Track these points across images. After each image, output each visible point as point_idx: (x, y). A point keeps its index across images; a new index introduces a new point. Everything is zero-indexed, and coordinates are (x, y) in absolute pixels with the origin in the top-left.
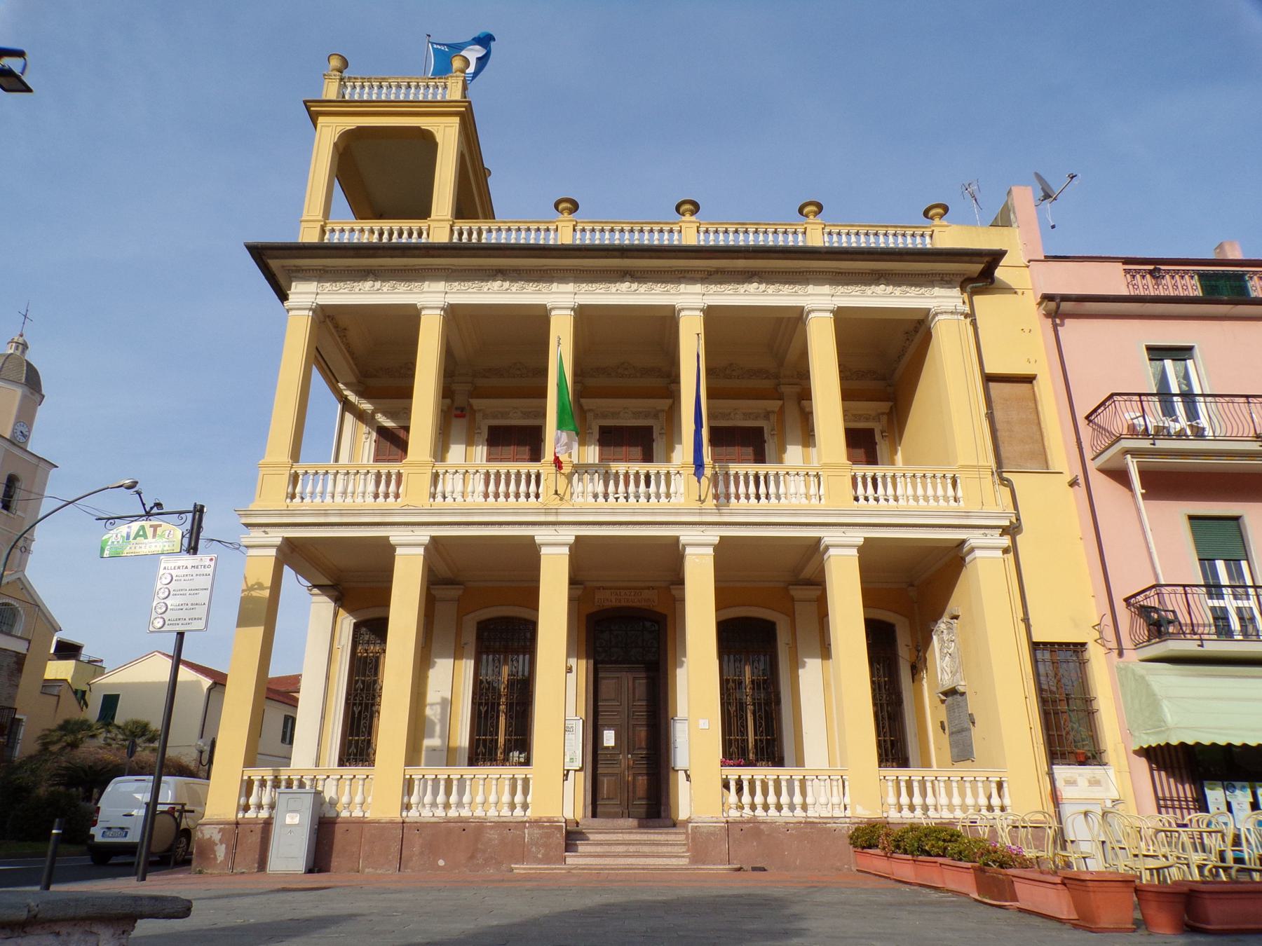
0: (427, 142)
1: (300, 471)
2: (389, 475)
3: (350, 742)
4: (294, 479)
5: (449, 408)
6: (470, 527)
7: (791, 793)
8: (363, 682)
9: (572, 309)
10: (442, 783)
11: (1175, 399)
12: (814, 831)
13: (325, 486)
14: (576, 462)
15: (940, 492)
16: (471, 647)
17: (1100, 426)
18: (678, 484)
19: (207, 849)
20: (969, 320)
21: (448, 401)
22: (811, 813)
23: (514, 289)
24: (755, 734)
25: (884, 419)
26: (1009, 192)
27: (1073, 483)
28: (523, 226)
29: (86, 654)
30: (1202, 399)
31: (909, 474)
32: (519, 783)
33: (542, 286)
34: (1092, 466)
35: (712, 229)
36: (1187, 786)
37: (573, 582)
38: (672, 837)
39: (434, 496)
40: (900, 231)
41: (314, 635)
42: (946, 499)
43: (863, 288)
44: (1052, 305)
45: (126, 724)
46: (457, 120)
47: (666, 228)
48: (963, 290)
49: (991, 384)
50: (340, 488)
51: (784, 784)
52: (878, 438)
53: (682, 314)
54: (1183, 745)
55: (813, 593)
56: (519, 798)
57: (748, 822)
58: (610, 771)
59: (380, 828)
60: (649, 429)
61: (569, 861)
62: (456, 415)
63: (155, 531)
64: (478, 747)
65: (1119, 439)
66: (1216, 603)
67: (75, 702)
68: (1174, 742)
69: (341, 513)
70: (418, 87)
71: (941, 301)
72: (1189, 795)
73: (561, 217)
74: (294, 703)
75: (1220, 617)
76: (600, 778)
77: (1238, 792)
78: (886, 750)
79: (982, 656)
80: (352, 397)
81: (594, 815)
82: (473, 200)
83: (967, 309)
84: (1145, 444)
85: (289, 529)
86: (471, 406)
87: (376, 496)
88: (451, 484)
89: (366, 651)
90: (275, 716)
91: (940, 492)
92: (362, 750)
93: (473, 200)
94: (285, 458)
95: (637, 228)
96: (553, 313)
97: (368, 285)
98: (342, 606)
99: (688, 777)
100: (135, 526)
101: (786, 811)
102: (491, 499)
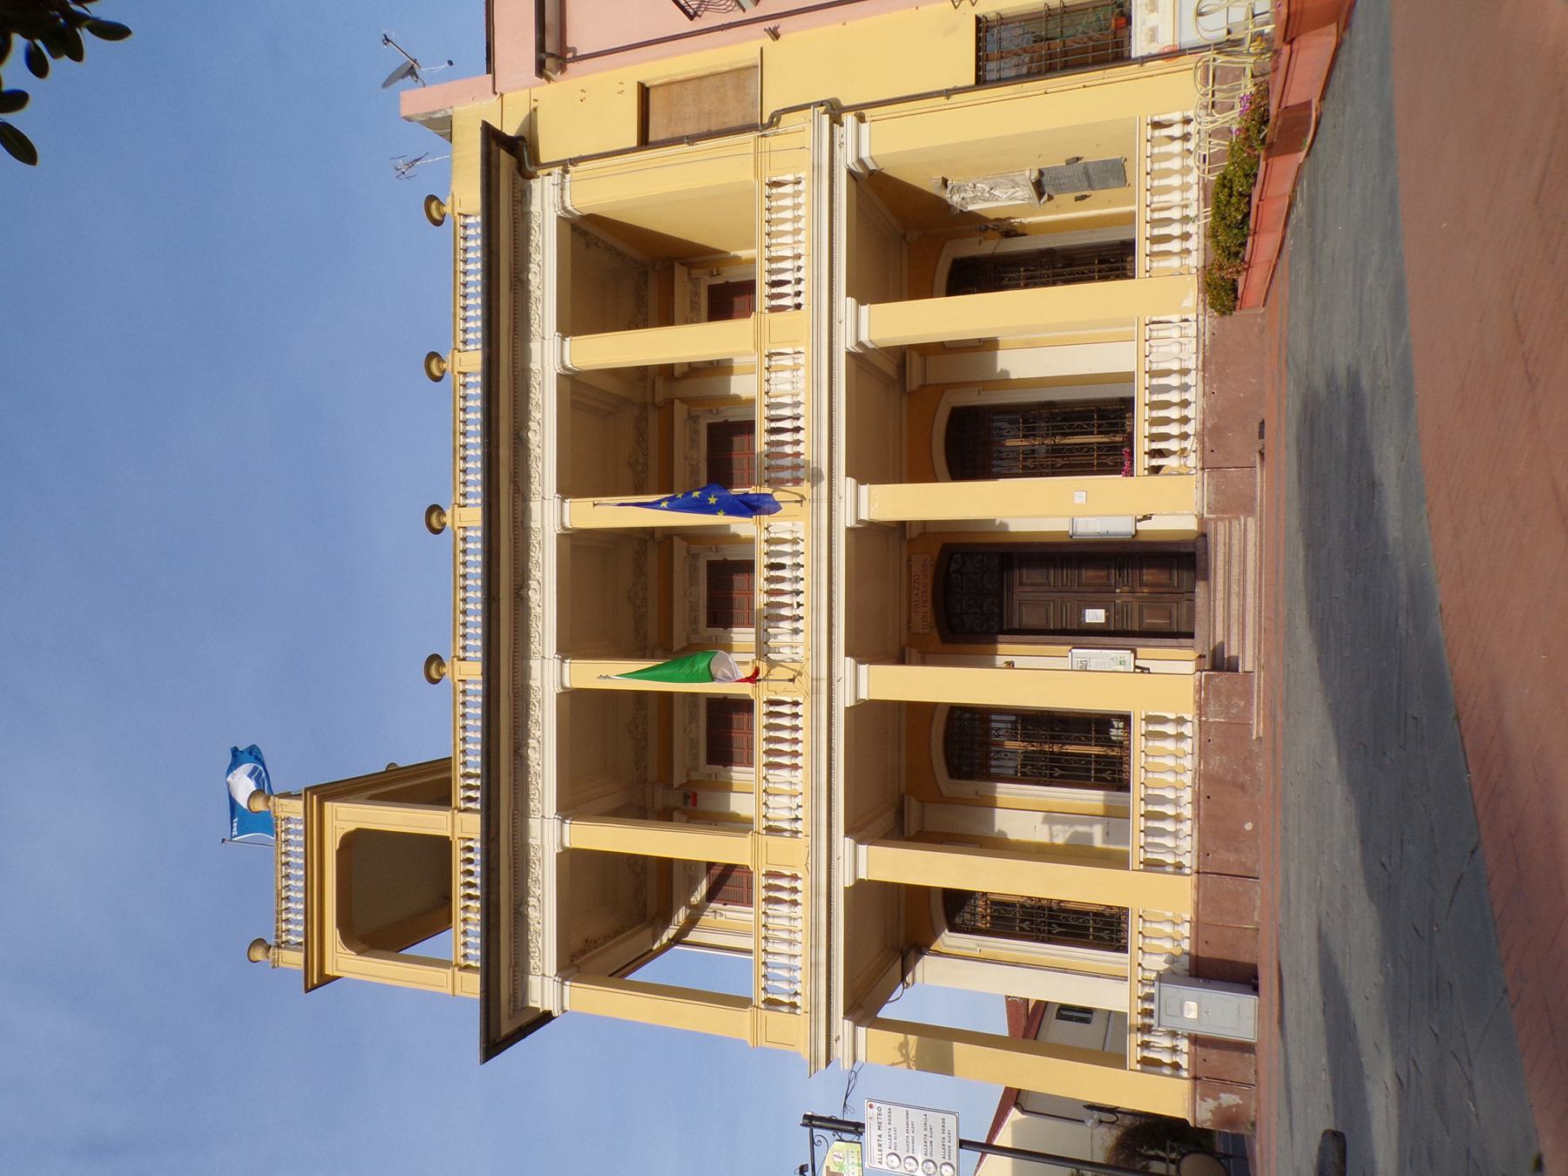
0: (355, 842)
1: (763, 996)
2: (768, 887)
3: (1096, 779)
4: (772, 1004)
5: (685, 813)
6: (835, 787)
8: (1022, 921)
10: (1150, 824)
12: (1214, 361)
15: (788, 202)
19: (1229, 1117)
20: (571, 168)
21: (676, 814)
22: (1191, 364)
23: (538, 733)
24: (1092, 433)
25: (696, 272)
26: (409, 119)
27: (775, 35)
28: (460, 722)
31: (767, 241)
32: (1151, 728)
35: (462, 489)
37: (901, 660)
38: (1221, 539)
40: (460, 256)
41: (963, 980)
42: (797, 194)
43: (533, 300)
44: (549, 62)
46: (328, 805)
47: (461, 546)
49: (652, 138)
51: (1155, 398)
53: (568, 525)
55: (914, 361)
56: (1170, 729)
57: (1202, 443)
58: (1136, 615)
59: (1204, 901)
60: (712, 565)
61: (1249, 667)
62: (693, 804)
64: (1104, 779)
69: (815, 947)
70: (287, 854)
71: (547, 203)
73: (448, 676)
74: (1042, 1006)
76: (1145, 627)
78: (1112, 270)
79: (993, 147)
80: (671, 932)
81: (1191, 635)
82: (428, 784)
83: (557, 170)
87: (794, 903)
88: (780, 810)
89: (984, 917)
90: (1057, 1030)
91: (788, 202)
92: (1107, 923)
93: (428, 784)
94: (746, 1015)
95: (461, 582)
96: (567, 685)
98: (928, 946)
99: (1146, 518)
102: (799, 761)
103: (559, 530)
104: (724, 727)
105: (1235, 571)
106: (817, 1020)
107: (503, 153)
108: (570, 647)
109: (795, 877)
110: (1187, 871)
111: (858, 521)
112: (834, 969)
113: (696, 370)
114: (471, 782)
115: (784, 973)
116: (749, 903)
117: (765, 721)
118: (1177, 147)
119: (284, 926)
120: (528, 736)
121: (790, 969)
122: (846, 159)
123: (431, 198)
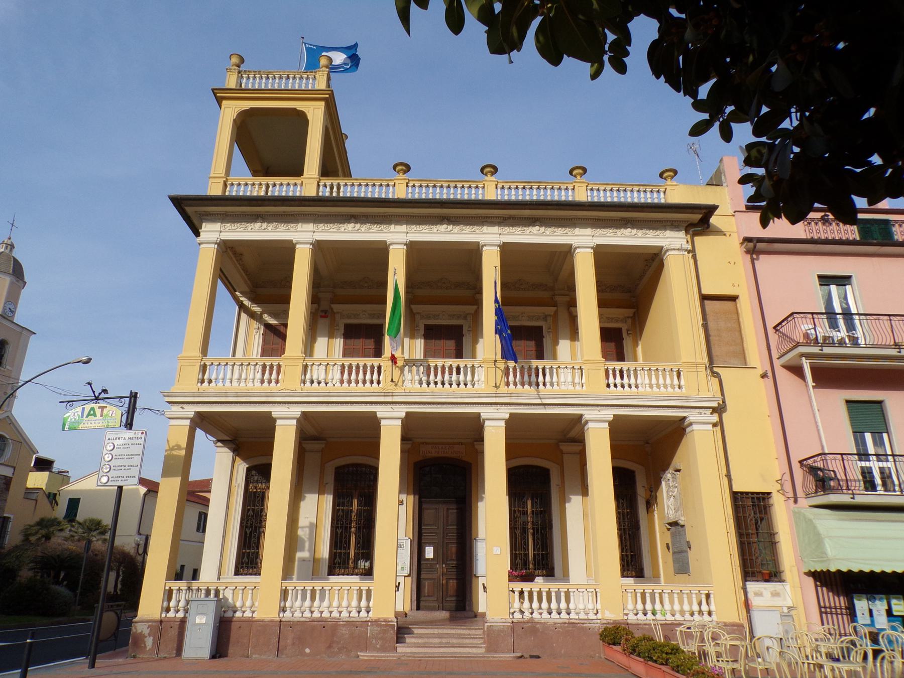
0: (301, 119)
1: (208, 363)
3: (335, 553)
4: (204, 368)
6: (330, 405)
7: (558, 601)
8: (253, 510)
9: (405, 244)
10: (309, 592)
11: (840, 312)
12: (574, 629)
13: (225, 375)
14: (407, 357)
15: (668, 381)
16: (331, 486)
17: (784, 334)
18: (480, 375)
19: (139, 640)
20: (690, 255)
21: (316, 306)
22: (573, 616)
23: (363, 229)
24: (534, 550)
25: (629, 321)
26: (721, 160)
27: (764, 376)
28: (370, 183)
29: (56, 467)
30: (857, 317)
32: (364, 592)
33: (384, 227)
34: (777, 364)
35: (506, 186)
36: (842, 598)
37: (404, 439)
38: (473, 632)
39: (304, 382)
40: (642, 188)
41: (220, 468)
42: (673, 386)
44: (751, 245)
45: (85, 522)
46: (323, 103)
47: (474, 185)
48: (687, 232)
50: (236, 376)
51: (553, 594)
52: (624, 335)
53: (484, 248)
54: (839, 571)
55: (576, 448)
56: (363, 603)
57: (528, 622)
58: (430, 576)
61: (399, 650)
62: (321, 316)
63: (102, 411)
64: (335, 558)
65: (798, 345)
66: (864, 464)
67: (49, 505)
68: (833, 569)
69: (237, 394)
70: (294, 78)
71: (671, 241)
72: (843, 605)
73: (398, 176)
74: (206, 502)
75: (867, 474)
76: (423, 582)
77: (877, 602)
79: (697, 498)
80: (246, 302)
81: (418, 608)
82: (334, 163)
83: (690, 247)
84: (815, 350)
85: (200, 405)
86: (332, 309)
87: (262, 382)
88: (318, 373)
89: (256, 488)
90: (192, 514)
91: (668, 381)
92: (252, 560)
93: (334, 163)
94: (197, 353)
95: (452, 185)
96: (391, 247)
97: (257, 225)
100: (88, 407)
101: (554, 614)
102: (345, 384)
103: (482, 243)
104: (365, 336)
105: (454, 641)
106: (194, 396)
107: (700, 216)
108: (413, 248)
109: (277, 382)
110: (281, 615)
111: (484, 420)
112: (223, 406)
113: (573, 320)
114: (335, 189)
115: (221, 376)
116: (263, 355)
117: (369, 364)
118: (696, 608)
119: (251, 76)
120: (362, 223)
121: (224, 379)
122: (692, 416)
123: (676, 172)
